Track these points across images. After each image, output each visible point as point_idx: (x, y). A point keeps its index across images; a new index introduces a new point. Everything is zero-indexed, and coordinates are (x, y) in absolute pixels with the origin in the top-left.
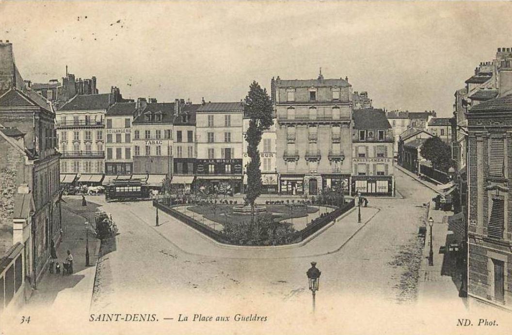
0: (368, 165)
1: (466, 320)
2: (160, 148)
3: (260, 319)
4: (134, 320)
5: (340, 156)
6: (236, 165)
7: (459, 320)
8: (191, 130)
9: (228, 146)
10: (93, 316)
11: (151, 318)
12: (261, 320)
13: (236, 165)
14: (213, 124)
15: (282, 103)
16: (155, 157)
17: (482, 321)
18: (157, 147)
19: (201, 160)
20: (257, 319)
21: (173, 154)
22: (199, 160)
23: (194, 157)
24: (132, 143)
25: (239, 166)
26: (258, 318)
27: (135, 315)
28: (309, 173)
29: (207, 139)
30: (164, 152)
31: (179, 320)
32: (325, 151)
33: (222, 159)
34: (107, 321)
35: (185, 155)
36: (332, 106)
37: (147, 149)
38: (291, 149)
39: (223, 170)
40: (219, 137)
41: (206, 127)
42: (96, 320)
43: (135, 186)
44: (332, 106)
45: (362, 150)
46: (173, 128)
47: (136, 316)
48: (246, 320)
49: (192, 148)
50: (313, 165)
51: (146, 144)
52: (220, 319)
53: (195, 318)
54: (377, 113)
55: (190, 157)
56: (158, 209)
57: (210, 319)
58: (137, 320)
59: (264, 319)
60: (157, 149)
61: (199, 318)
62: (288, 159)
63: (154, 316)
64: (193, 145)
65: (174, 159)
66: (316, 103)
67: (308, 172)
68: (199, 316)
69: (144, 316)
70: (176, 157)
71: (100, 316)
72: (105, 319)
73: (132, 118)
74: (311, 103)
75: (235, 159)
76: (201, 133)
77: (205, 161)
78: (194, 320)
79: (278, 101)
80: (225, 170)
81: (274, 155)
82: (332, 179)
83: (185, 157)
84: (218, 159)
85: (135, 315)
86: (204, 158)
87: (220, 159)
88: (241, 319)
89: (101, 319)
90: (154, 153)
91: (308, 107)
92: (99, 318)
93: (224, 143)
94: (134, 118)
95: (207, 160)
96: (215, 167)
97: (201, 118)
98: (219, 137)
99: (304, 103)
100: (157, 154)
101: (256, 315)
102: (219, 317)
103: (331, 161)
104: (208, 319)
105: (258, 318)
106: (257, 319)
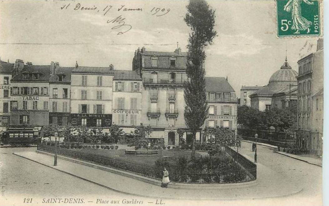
0: (231, 121)
1: (51, 202)
2: (36, 104)
3: (138, 203)
4: (70, 203)
5: (157, 113)
6: (107, 120)
7: (56, 202)
8: (67, 88)
9: (84, 102)
10: (44, 199)
11: (80, 201)
12: (139, 203)
13: (107, 120)
14: (86, 84)
15: (146, 69)
16: (32, 111)
17: (135, 203)
18: (34, 102)
19: (75, 114)
20: (136, 202)
21: (48, 108)
22: (74, 114)
23: (68, 111)
24: (10, 98)
25: (109, 121)
26: (138, 202)
27: (70, 199)
28: (168, 127)
29: (81, 96)
30: (40, 107)
31: (156, 204)
32: (163, 111)
33: (94, 114)
34: (53, 203)
35: (60, 110)
36: (152, 72)
37: (24, 103)
38: (154, 108)
39: (94, 124)
40: (92, 94)
41: (80, 86)
42: (46, 202)
43: (27, 133)
44: (152, 72)
45: (226, 111)
46: (50, 86)
47: (71, 200)
48: (105, 203)
49: (66, 103)
50: (171, 121)
51: (24, 99)
52: (114, 202)
53: (97, 201)
54: (51, 75)
55: (65, 111)
56: (237, 152)
57: (107, 202)
58: (72, 203)
59: (141, 203)
60: (34, 105)
61: (100, 201)
62: (169, 115)
63: (82, 200)
64: (68, 101)
65: (50, 113)
66: (175, 69)
67: (167, 127)
68: (100, 200)
69: (76, 200)
70: (52, 112)
71: (49, 199)
72: (52, 202)
73: (10, 76)
74: (171, 69)
75: (105, 115)
76: (75, 91)
77: (78, 116)
78: (97, 203)
79: (143, 65)
80: (96, 123)
81: (139, 112)
82: (187, 132)
83: (60, 112)
84: (90, 114)
85: (70, 199)
86: (77, 113)
87: (92, 114)
88: (126, 202)
89: (50, 201)
90: (31, 107)
91: (169, 72)
92: (49, 201)
93: (96, 100)
94: (13, 76)
95: (80, 115)
96: (102, 121)
97: (76, 79)
98: (92, 94)
99: (166, 69)
100: (34, 108)
101: (136, 200)
102: (113, 201)
103: (168, 117)
104: (106, 202)
105: (138, 202)
106: (136, 202)
